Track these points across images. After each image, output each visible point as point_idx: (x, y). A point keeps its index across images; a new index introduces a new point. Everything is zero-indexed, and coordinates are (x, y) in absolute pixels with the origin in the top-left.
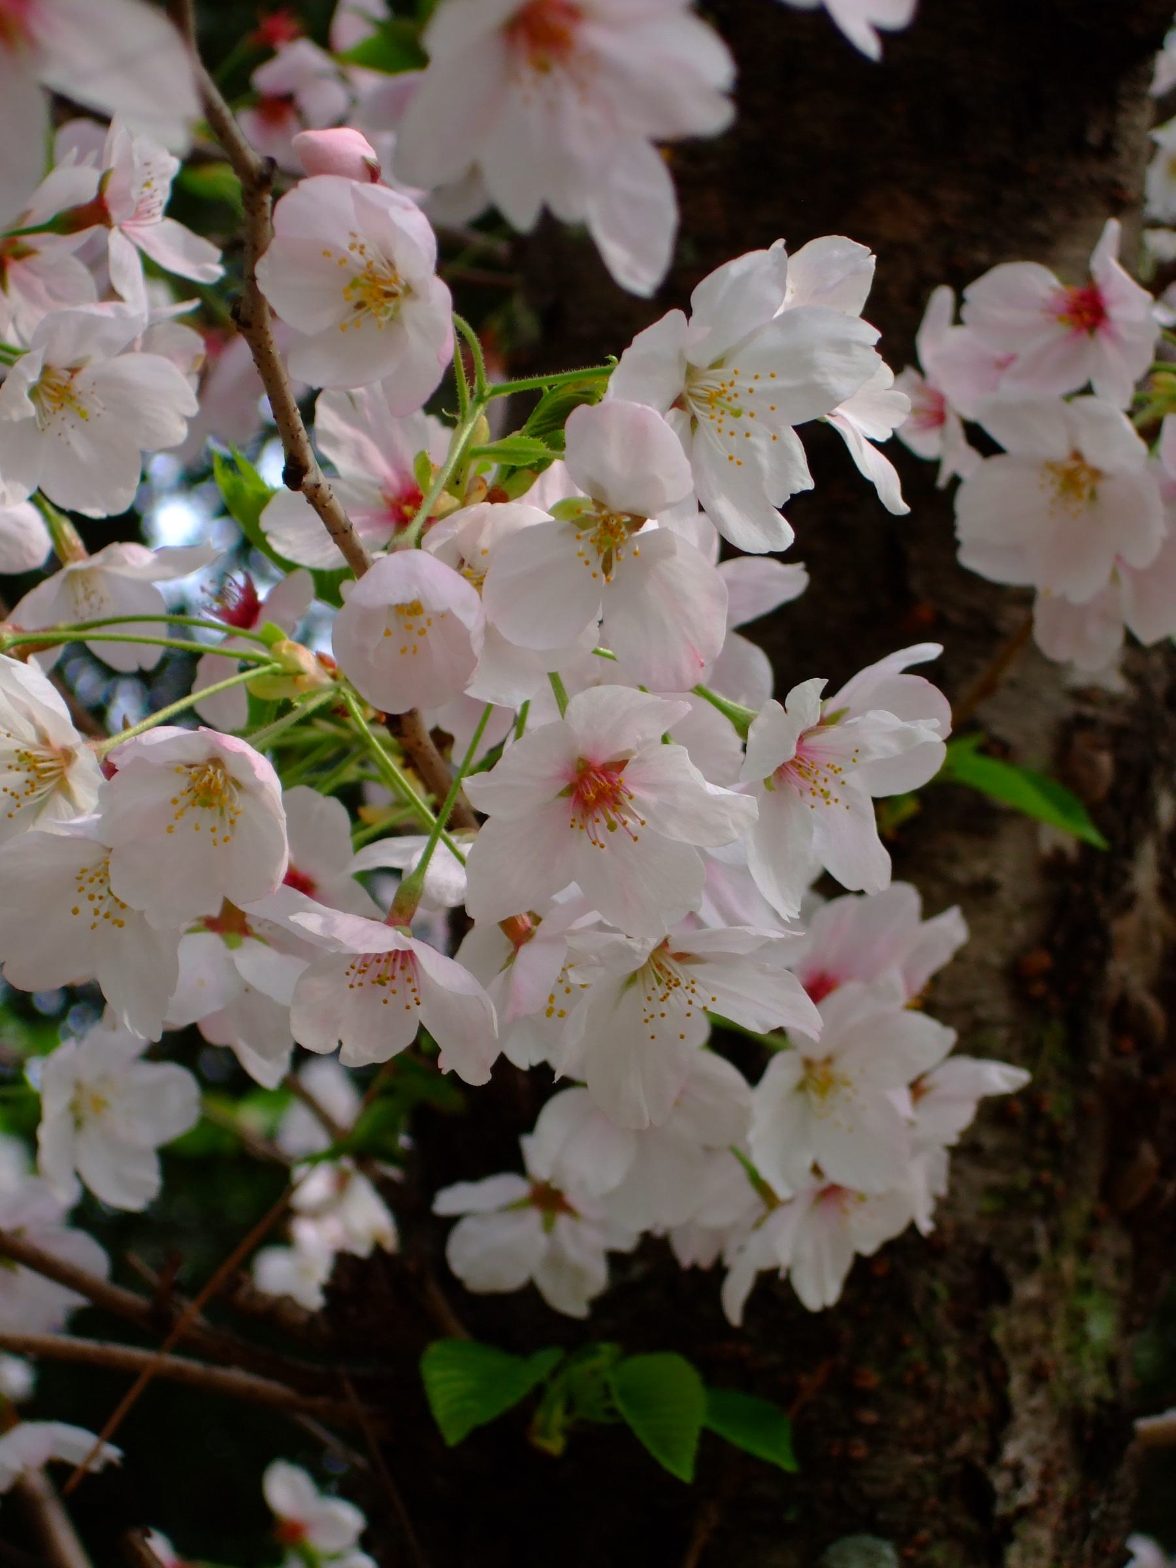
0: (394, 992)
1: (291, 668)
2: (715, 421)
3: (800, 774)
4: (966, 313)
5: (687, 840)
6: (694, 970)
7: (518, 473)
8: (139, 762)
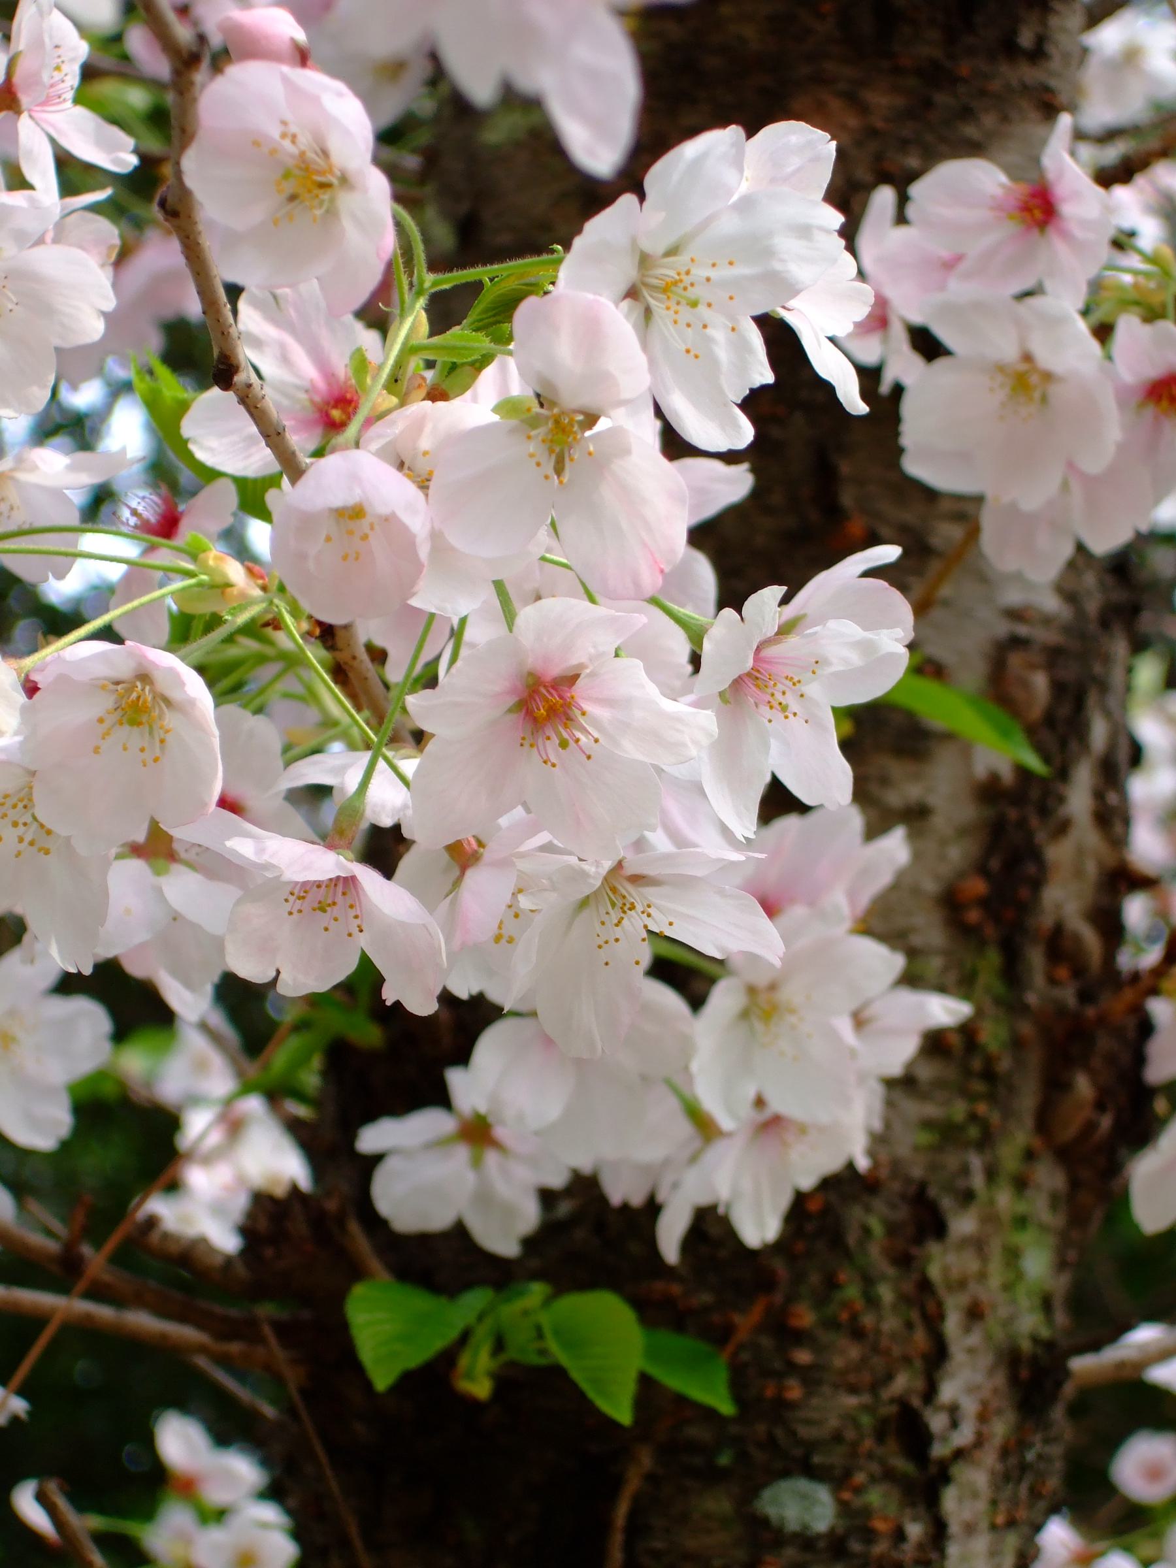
0: (336, 919)
1: (219, 580)
2: (671, 312)
3: (757, 686)
4: (911, 211)
5: (641, 757)
6: (650, 892)
7: (458, 371)
8: (62, 679)
